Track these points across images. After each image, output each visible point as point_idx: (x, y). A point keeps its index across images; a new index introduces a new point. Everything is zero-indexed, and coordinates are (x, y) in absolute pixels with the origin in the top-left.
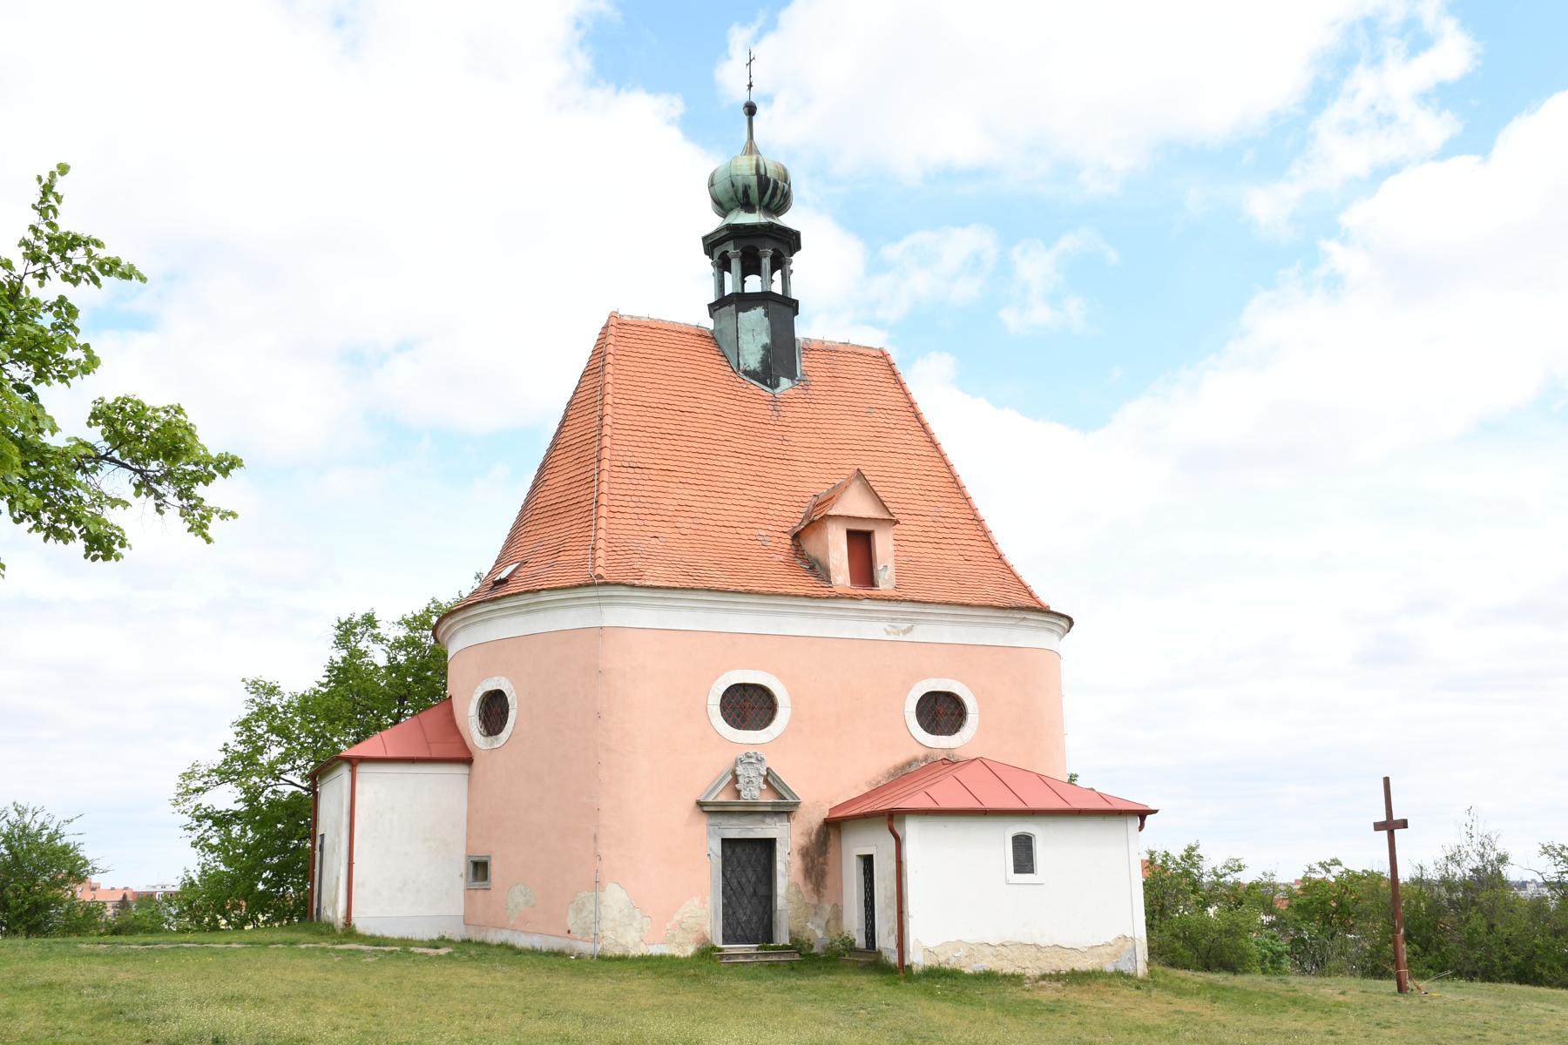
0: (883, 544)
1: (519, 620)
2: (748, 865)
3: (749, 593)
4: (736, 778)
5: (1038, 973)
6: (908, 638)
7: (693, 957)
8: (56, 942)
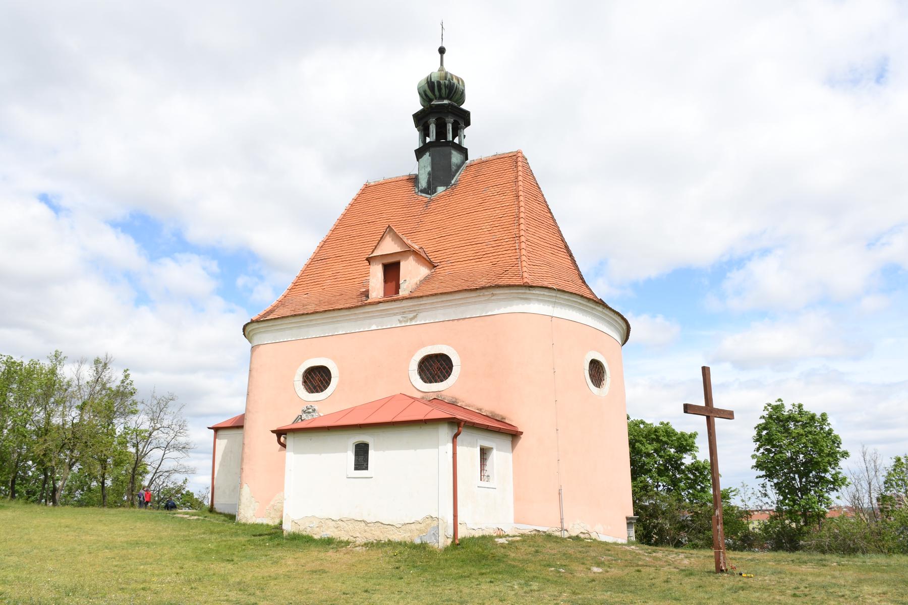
6: (413, 323)
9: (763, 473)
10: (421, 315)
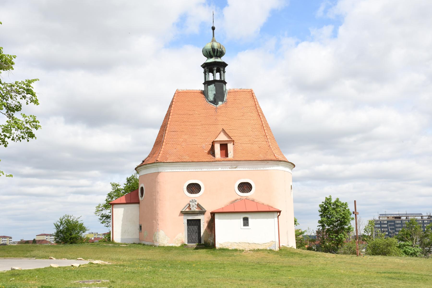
0: (230, 147)
1: (145, 171)
2: (193, 225)
3: (192, 162)
4: (190, 206)
5: (249, 249)
8: (79, 245)
9: (320, 224)
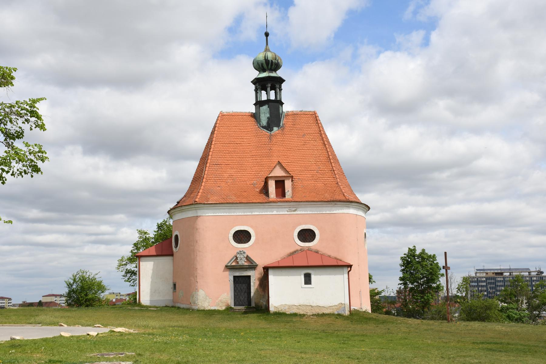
0: (288, 184)
1: (180, 214)
2: (241, 284)
4: (237, 258)
5: (311, 314)
7: (224, 310)
9: (402, 282)
10: (298, 209)
